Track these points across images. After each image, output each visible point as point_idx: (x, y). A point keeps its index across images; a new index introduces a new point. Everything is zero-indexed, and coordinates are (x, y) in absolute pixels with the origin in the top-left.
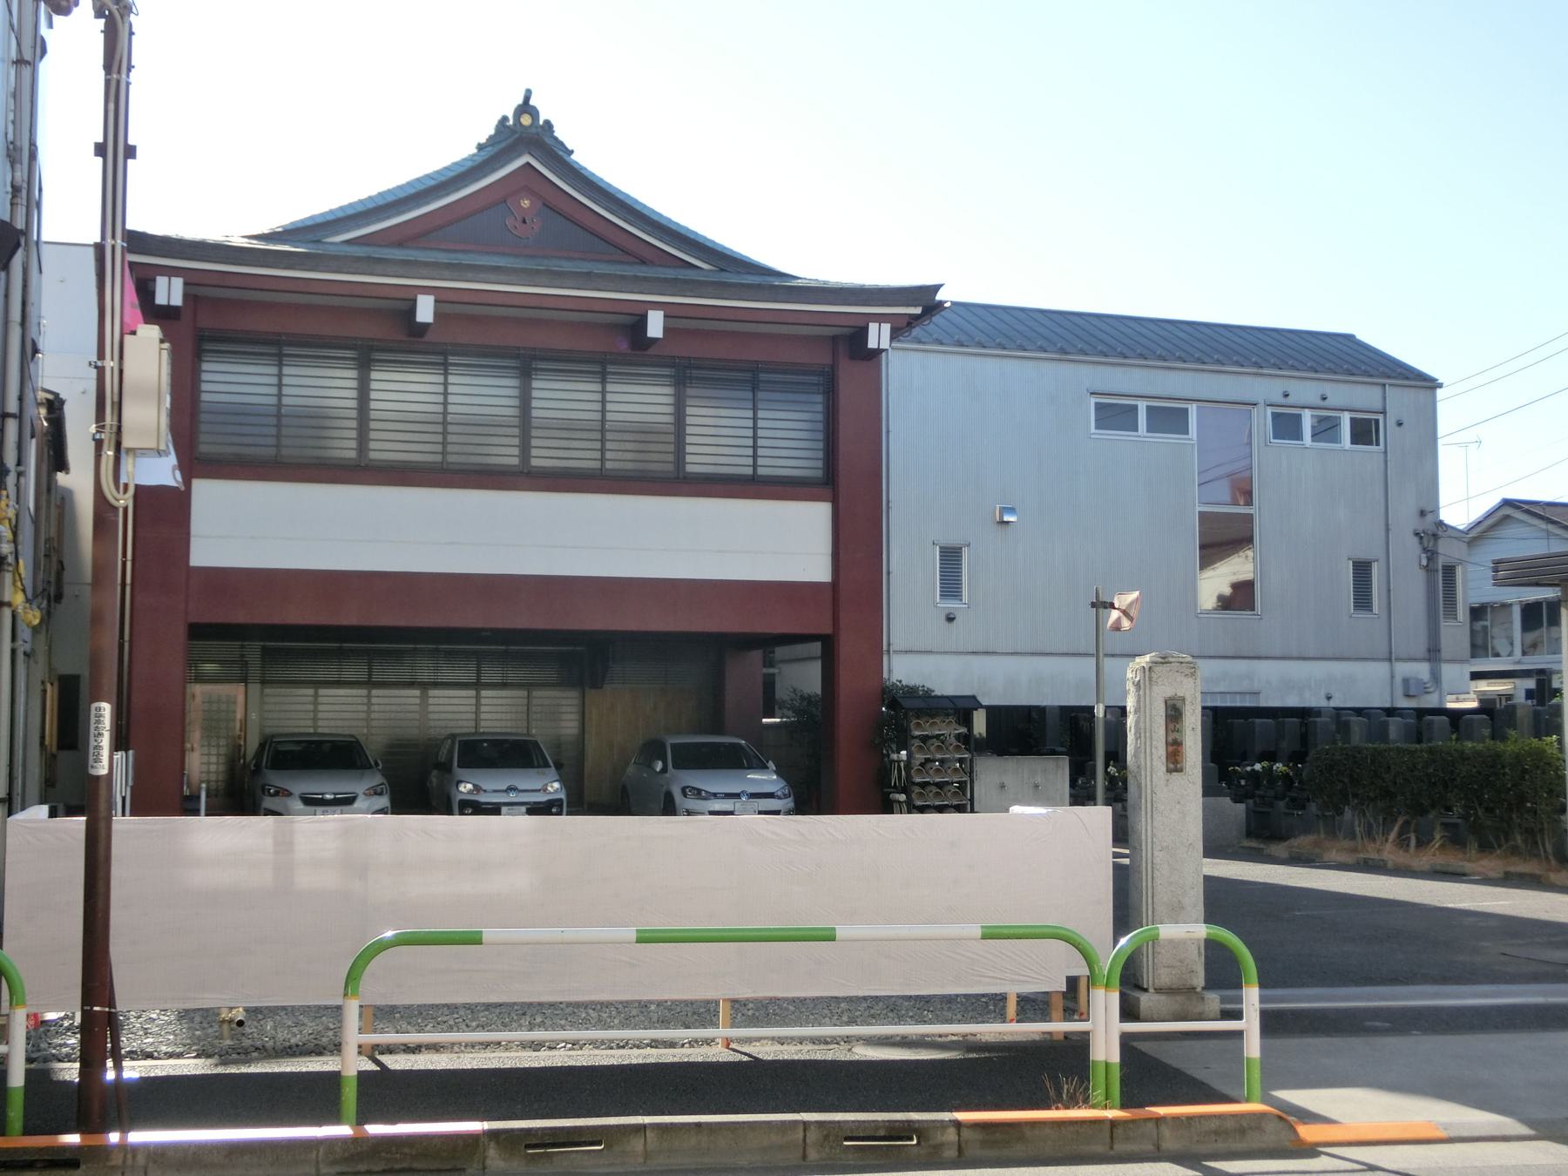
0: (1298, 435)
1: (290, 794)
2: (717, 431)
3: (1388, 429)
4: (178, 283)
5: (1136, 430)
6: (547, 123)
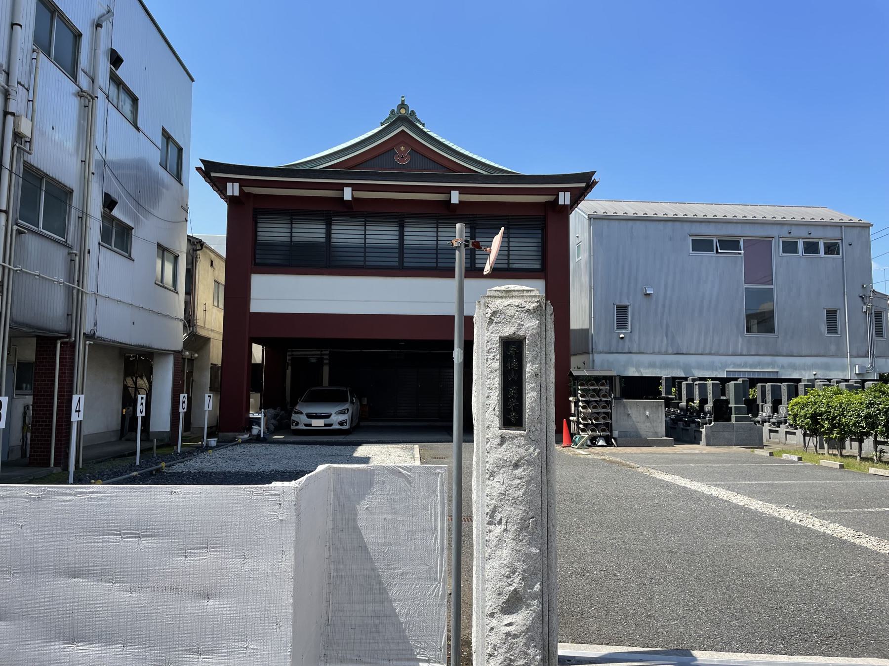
1: (301, 413)
3: (844, 248)
4: (568, 194)
5: (796, 252)
6: (413, 111)
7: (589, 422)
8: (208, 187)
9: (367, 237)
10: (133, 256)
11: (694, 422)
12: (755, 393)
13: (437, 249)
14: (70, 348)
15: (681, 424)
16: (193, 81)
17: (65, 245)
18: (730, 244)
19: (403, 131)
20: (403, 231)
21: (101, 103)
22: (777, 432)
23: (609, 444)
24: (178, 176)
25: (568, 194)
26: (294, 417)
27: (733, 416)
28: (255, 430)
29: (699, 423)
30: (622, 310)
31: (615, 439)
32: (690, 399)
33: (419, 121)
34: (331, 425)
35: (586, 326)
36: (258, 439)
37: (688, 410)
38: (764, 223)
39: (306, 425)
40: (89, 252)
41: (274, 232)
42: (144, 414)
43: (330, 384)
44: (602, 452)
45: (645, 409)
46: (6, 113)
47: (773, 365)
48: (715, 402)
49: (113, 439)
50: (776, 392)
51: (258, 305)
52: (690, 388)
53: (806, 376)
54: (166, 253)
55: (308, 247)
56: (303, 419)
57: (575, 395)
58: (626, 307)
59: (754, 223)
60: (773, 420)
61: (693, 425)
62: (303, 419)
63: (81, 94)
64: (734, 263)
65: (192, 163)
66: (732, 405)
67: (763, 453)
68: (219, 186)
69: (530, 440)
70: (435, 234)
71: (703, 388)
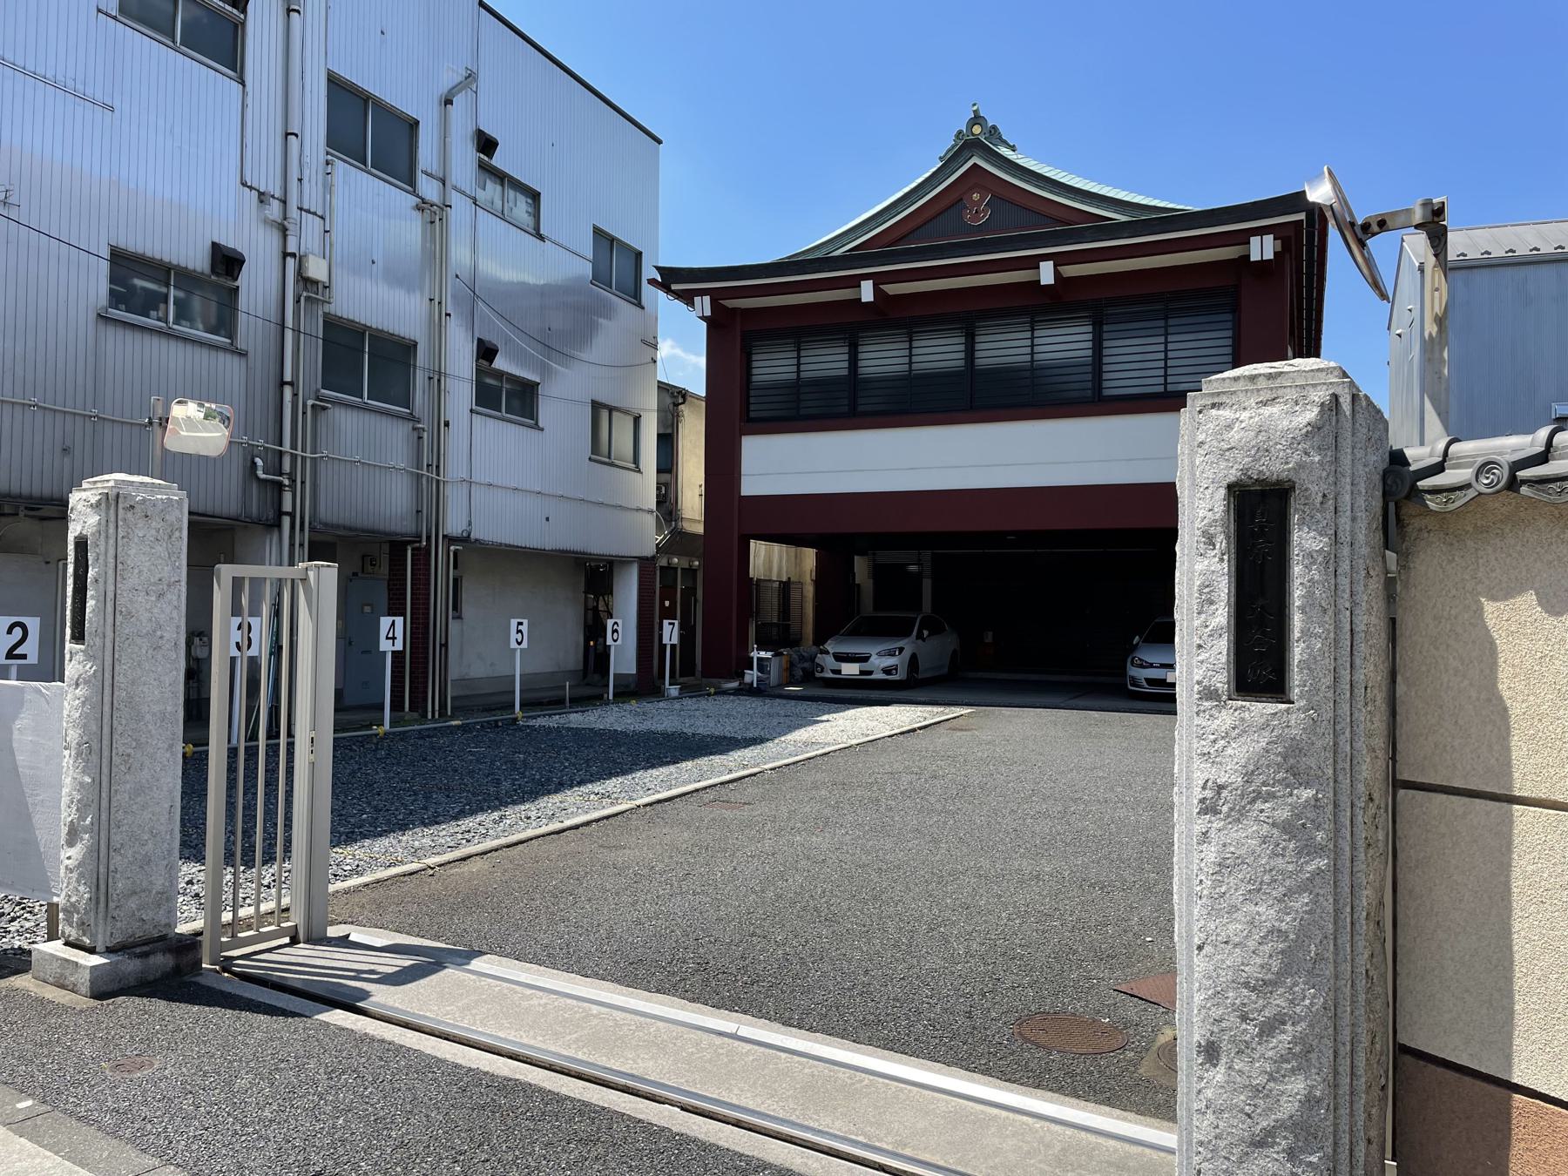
6: (994, 127)
14: (422, 556)
16: (660, 142)
17: (411, 418)
21: (460, 209)
24: (635, 297)
25: (1269, 239)
26: (820, 658)
28: (752, 676)
34: (870, 673)
36: (748, 691)
39: (834, 671)
40: (447, 424)
41: (773, 366)
43: (876, 608)
46: (285, 255)
51: (754, 483)
54: (615, 414)
56: (829, 662)
62: (829, 662)
63: (423, 206)
65: (649, 272)
68: (687, 298)
69: (89, 657)
70: (906, 352)
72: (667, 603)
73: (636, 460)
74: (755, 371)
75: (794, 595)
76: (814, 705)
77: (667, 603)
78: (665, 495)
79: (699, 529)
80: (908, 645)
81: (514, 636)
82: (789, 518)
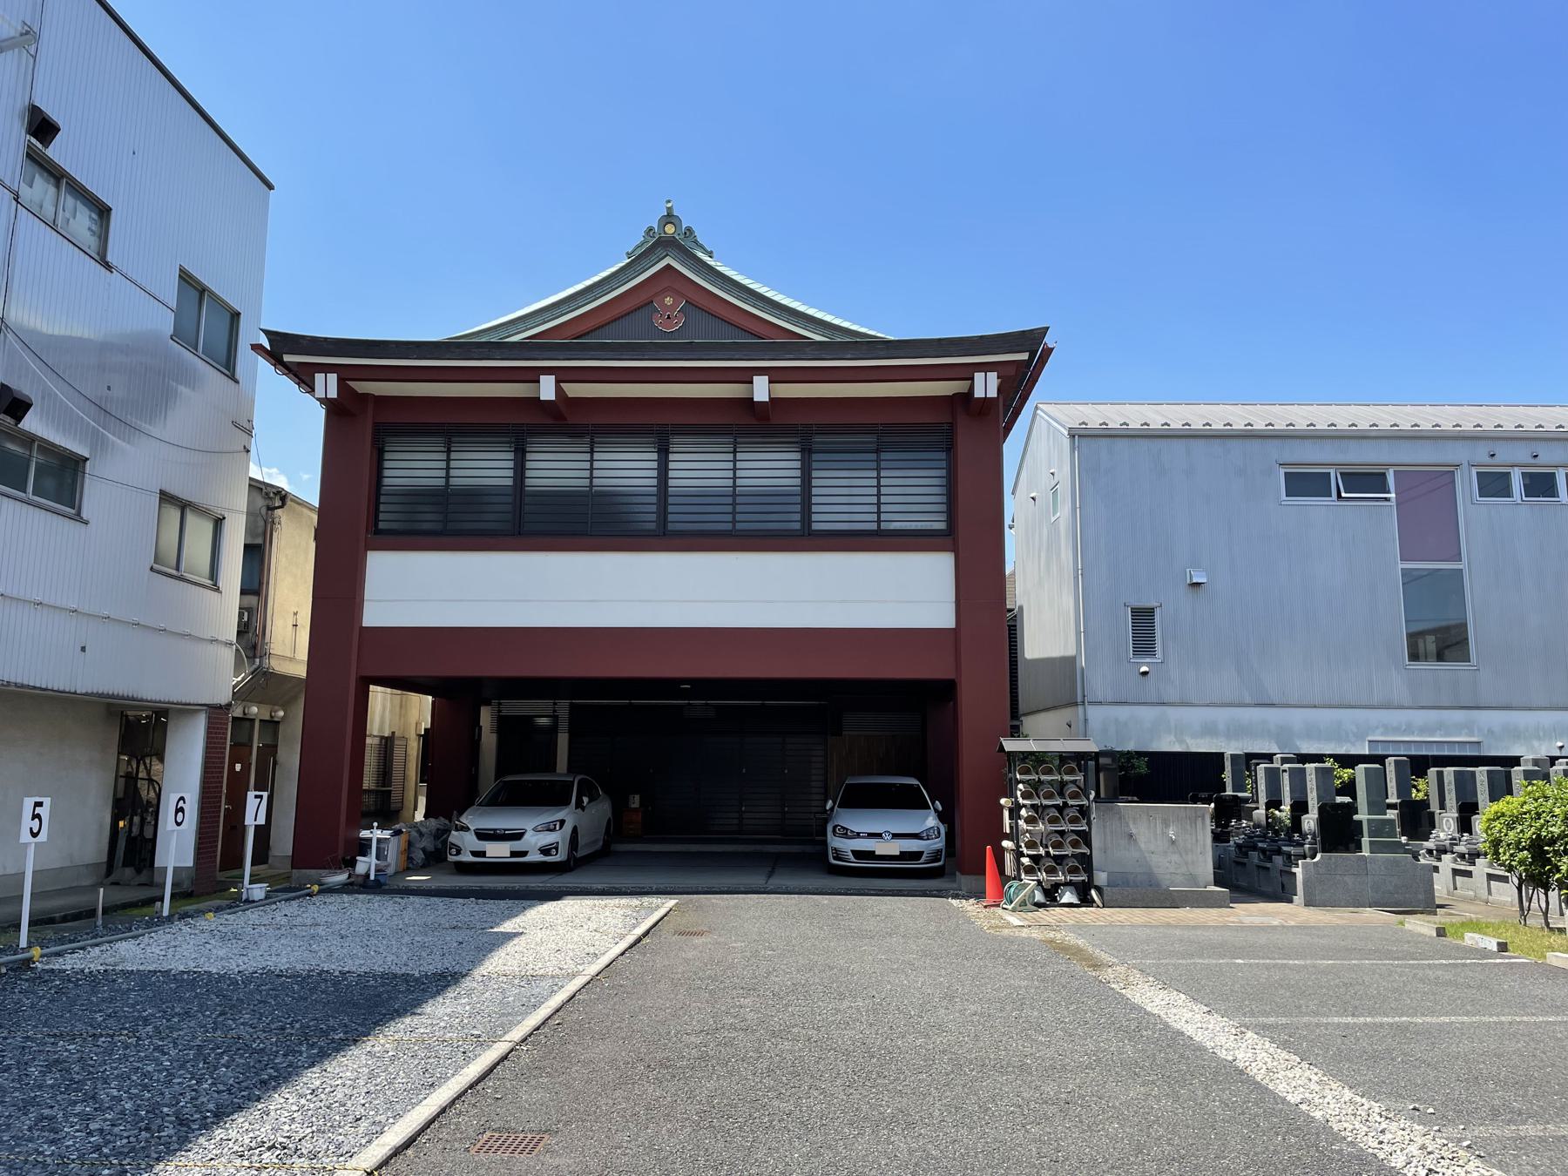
0: (1507, 493)
1: (467, 829)
2: (844, 492)
4: (993, 377)
6: (689, 229)
7: (1042, 851)
8: (287, 384)
9: (596, 473)
10: (84, 515)
11: (1279, 852)
12: (1424, 789)
13: (734, 495)
15: (1254, 856)
16: (271, 187)
18: (1366, 481)
19: (668, 267)
20: (667, 461)
22: (1468, 874)
23: (1086, 901)
24: (228, 366)
25: (993, 377)
26: (455, 837)
27: (1365, 840)
28: (366, 865)
29: (1289, 855)
30: (1143, 618)
31: (1099, 889)
32: (1274, 803)
33: (702, 247)
34: (524, 854)
35: (1071, 652)
36: (364, 886)
37: (1272, 824)
38: (1437, 437)
41: (413, 468)
42: (262, 821)
44: (1068, 922)
45: (1166, 824)
47: (1469, 727)
48: (1321, 810)
49: (87, 882)
50: (1465, 786)
51: (378, 612)
52: (1273, 777)
53: (1529, 752)
55: (475, 496)
57: (1011, 794)
58: (1150, 612)
59: (1415, 437)
60: (1461, 848)
61: (1278, 860)
64: (1379, 519)
65: (251, 333)
66: (1362, 816)
67: (1422, 926)
68: (303, 377)
71: (1298, 778)
72: (238, 767)
73: (214, 573)
74: (387, 473)
75: (398, 753)
76: (491, 905)
77: (238, 767)
78: (247, 625)
79: (301, 671)
80: (567, 814)
81: (27, 823)
82: (413, 658)
